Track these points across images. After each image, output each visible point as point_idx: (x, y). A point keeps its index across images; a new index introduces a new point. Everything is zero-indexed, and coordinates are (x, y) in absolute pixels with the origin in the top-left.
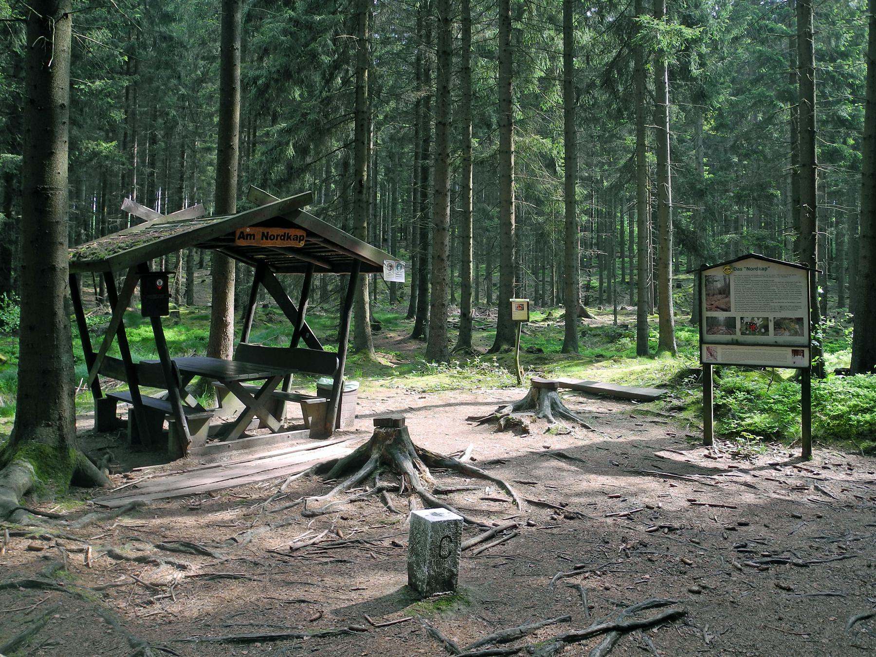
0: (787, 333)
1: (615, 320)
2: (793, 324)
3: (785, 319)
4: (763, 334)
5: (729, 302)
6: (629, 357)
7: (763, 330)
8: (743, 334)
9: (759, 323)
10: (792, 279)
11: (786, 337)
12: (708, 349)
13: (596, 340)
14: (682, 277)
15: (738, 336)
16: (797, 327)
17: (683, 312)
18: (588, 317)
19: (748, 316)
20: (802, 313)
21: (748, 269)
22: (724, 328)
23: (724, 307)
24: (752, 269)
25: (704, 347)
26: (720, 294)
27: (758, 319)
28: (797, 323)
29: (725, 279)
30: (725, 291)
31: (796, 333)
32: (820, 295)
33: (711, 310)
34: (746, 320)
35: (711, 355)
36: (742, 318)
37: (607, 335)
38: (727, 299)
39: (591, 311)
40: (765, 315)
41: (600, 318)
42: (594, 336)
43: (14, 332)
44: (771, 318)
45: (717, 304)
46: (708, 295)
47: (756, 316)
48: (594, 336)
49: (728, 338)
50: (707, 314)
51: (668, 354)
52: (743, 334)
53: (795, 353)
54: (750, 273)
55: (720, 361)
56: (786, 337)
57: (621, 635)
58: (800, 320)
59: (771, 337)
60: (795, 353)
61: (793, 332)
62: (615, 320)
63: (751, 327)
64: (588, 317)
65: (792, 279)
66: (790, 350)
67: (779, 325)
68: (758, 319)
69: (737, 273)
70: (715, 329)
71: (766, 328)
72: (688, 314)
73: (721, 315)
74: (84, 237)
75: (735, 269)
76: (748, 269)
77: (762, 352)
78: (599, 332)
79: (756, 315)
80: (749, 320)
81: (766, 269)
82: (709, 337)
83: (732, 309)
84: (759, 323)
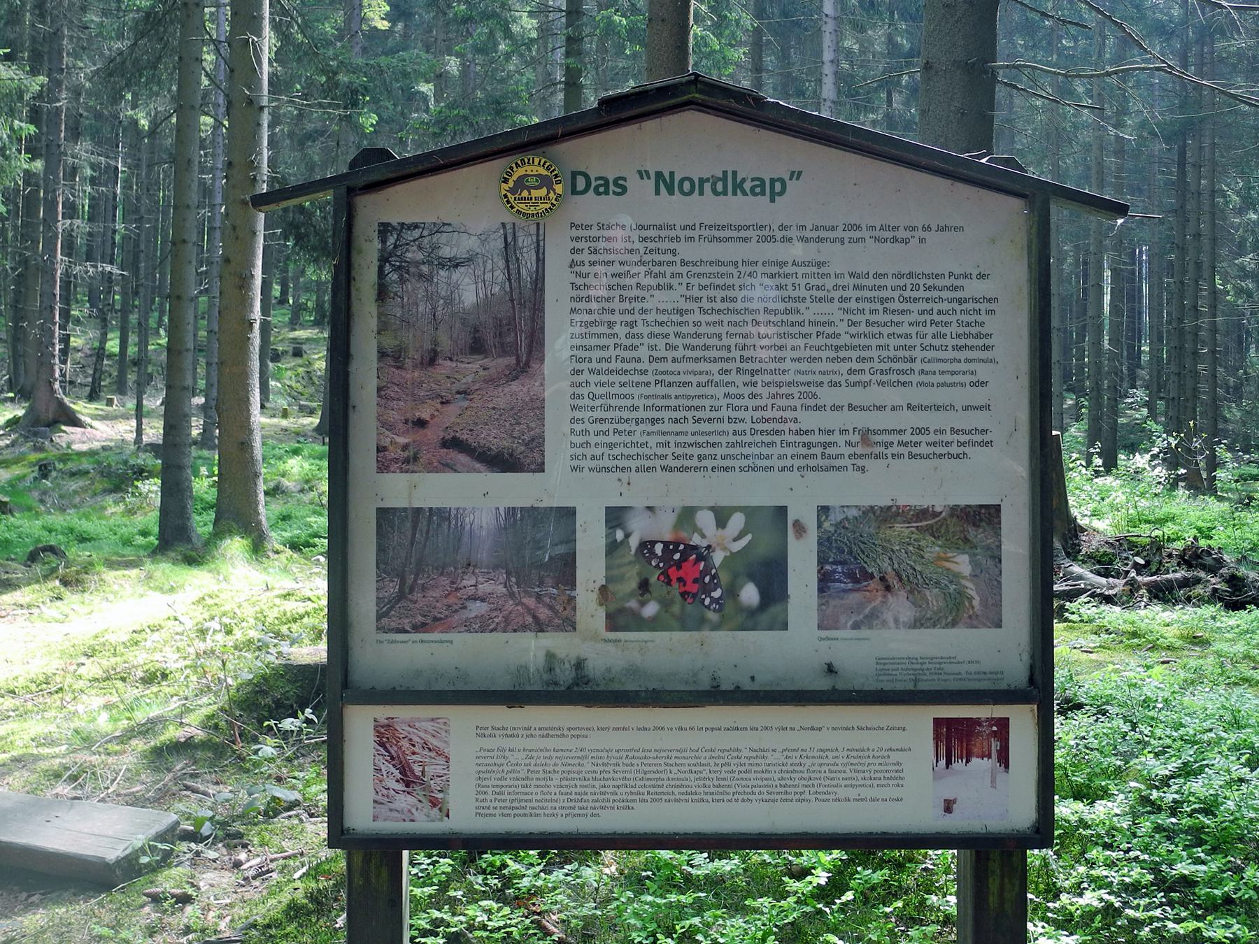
0: (900, 606)
1: (139, 431)
2: (933, 550)
3: (888, 515)
5: (537, 406)
6: (111, 565)
7: (750, 594)
9: (724, 543)
10: (938, 256)
11: (894, 640)
12: (385, 736)
13: (73, 485)
14: (301, 334)
15: (591, 643)
16: (962, 564)
17: (302, 408)
18: (75, 422)
19: (658, 500)
23: (493, 438)
24: (694, 187)
25: (361, 723)
26: (477, 347)
28: (965, 543)
29: (509, 249)
30: (511, 334)
31: (955, 611)
32: (1204, 344)
33: (410, 462)
34: (639, 528)
35: (409, 779)
36: (615, 517)
37: (106, 472)
39: (82, 408)
40: (761, 491)
41: (102, 428)
42: (73, 474)
44: (802, 511)
45: (451, 418)
46: (391, 357)
47: (710, 498)
48: (73, 474)
49: (530, 650)
51: (235, 546)
53: (955, 740)
54: (675, 209)
55: (464, 816)
56: (894, 640)
58: (987, 516)
59: (802, 637)
60: (955, 740)
61: (933, 596)
62: (139, 431)
63: (676, 573)
64: (75, 422)
65: (938, 256)
66: (918, 723)
67: (853, 562)
69: (588, 207)
70: (434, 596)
72: (311, 412)
75: (579, 183)
76: (665, 183)
77: (744, 742)
78: (86, 464)
80: (663, 528)
81: (771, 189)
83: (557, 451)
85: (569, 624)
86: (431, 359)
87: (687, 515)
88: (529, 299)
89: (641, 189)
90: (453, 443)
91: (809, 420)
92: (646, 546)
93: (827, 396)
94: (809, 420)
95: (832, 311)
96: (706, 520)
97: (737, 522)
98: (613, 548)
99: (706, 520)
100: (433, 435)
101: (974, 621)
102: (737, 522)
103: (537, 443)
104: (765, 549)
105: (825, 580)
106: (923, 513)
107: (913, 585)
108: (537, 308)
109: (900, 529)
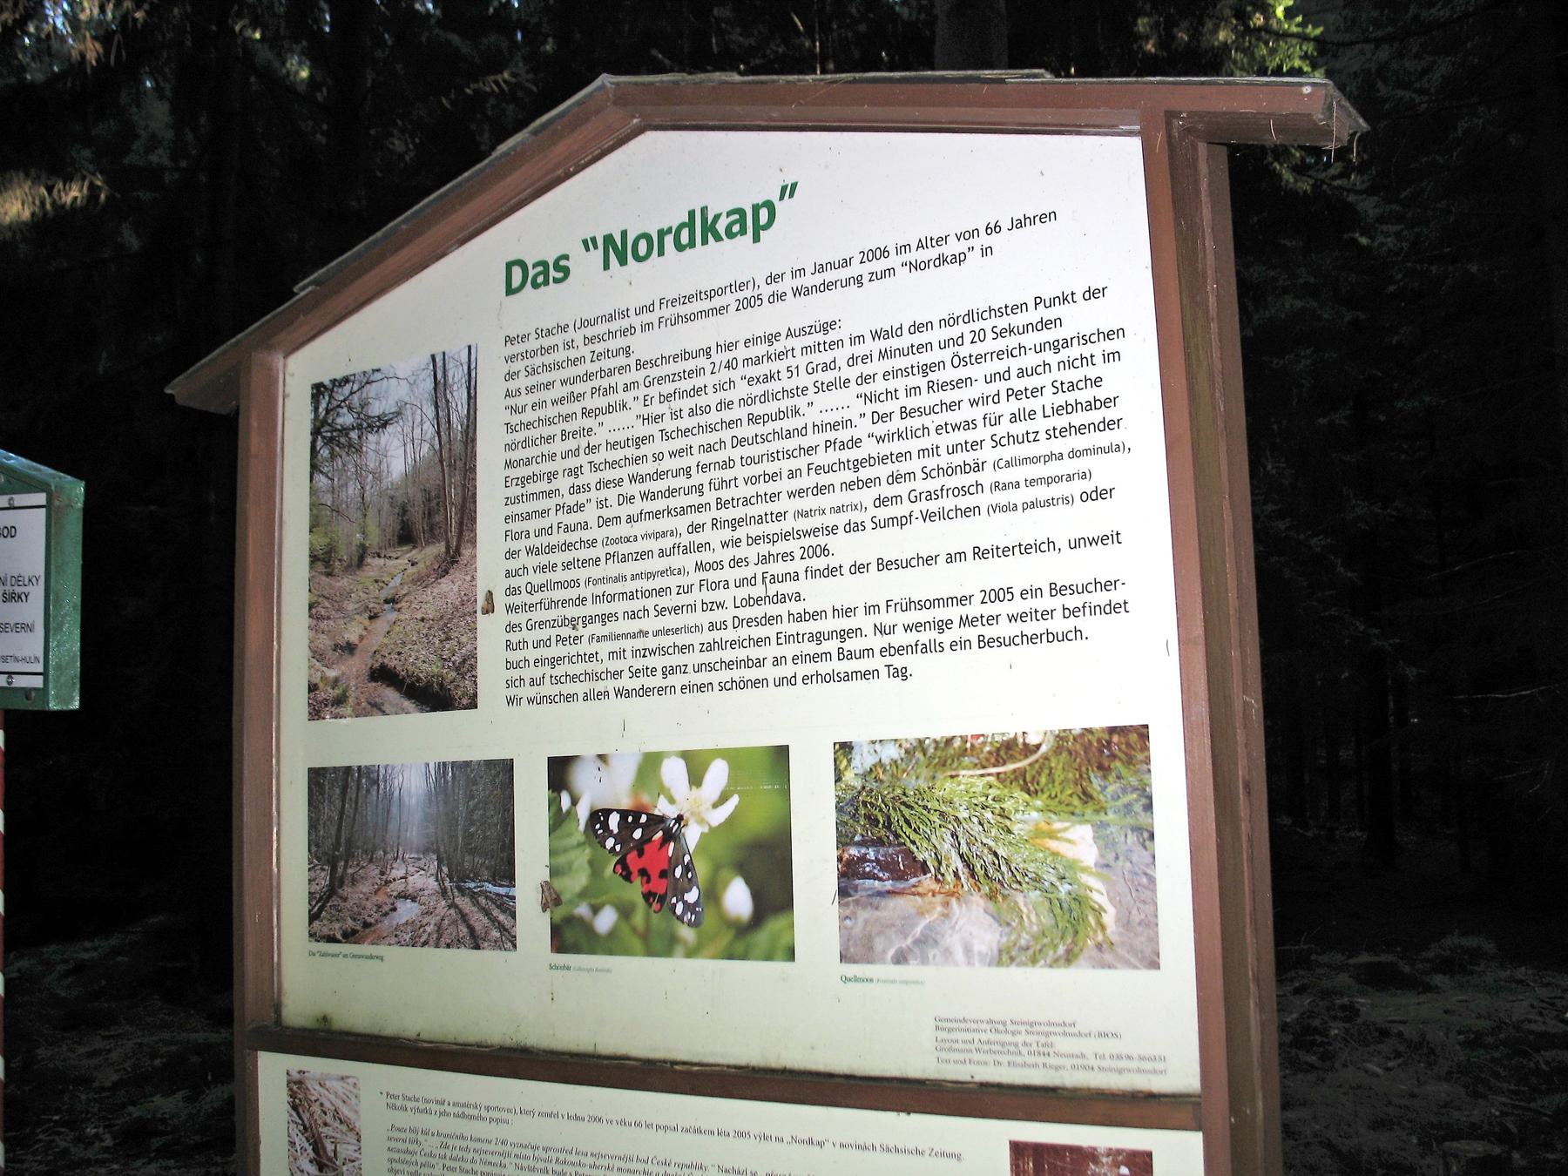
2: (1027, 816)
3: (944, 755)
4: (742, 940)
5: (1110, 1152)
7: (738, 898)
9: (702, 811)
16: (1079, 842)
21: (617, 249)
23: (423, 663)
26: (406, 537)
27: (696, 767)
31: (1069, 932)
36: (559, 771)
40: (746, 721)
52: (569, 936)
57: (1376, 48)
58: (1120, 749)
68: (696, 767)
71: (767, 863)
73: (407, 748)
74: (614, 821)
83: (490, 677)
87: (650, 764)
88: (457, 455)
89: (586, 264)
90: (383, 674)
91: (818, 594)
92: (599, 817)
93: (845, 549)
94: (818, 594)
95: (846, 402)
96: (674, 772)
97: (717, 774)
98: (559, 820)
99: (674, 772)
101: (1107, 954)
102: (717, 774)
103: (467, 666)
104: (758, 822)
105: (849, 872)
106: (1008, 749)
108: (469, 470)
109: (970, 781)
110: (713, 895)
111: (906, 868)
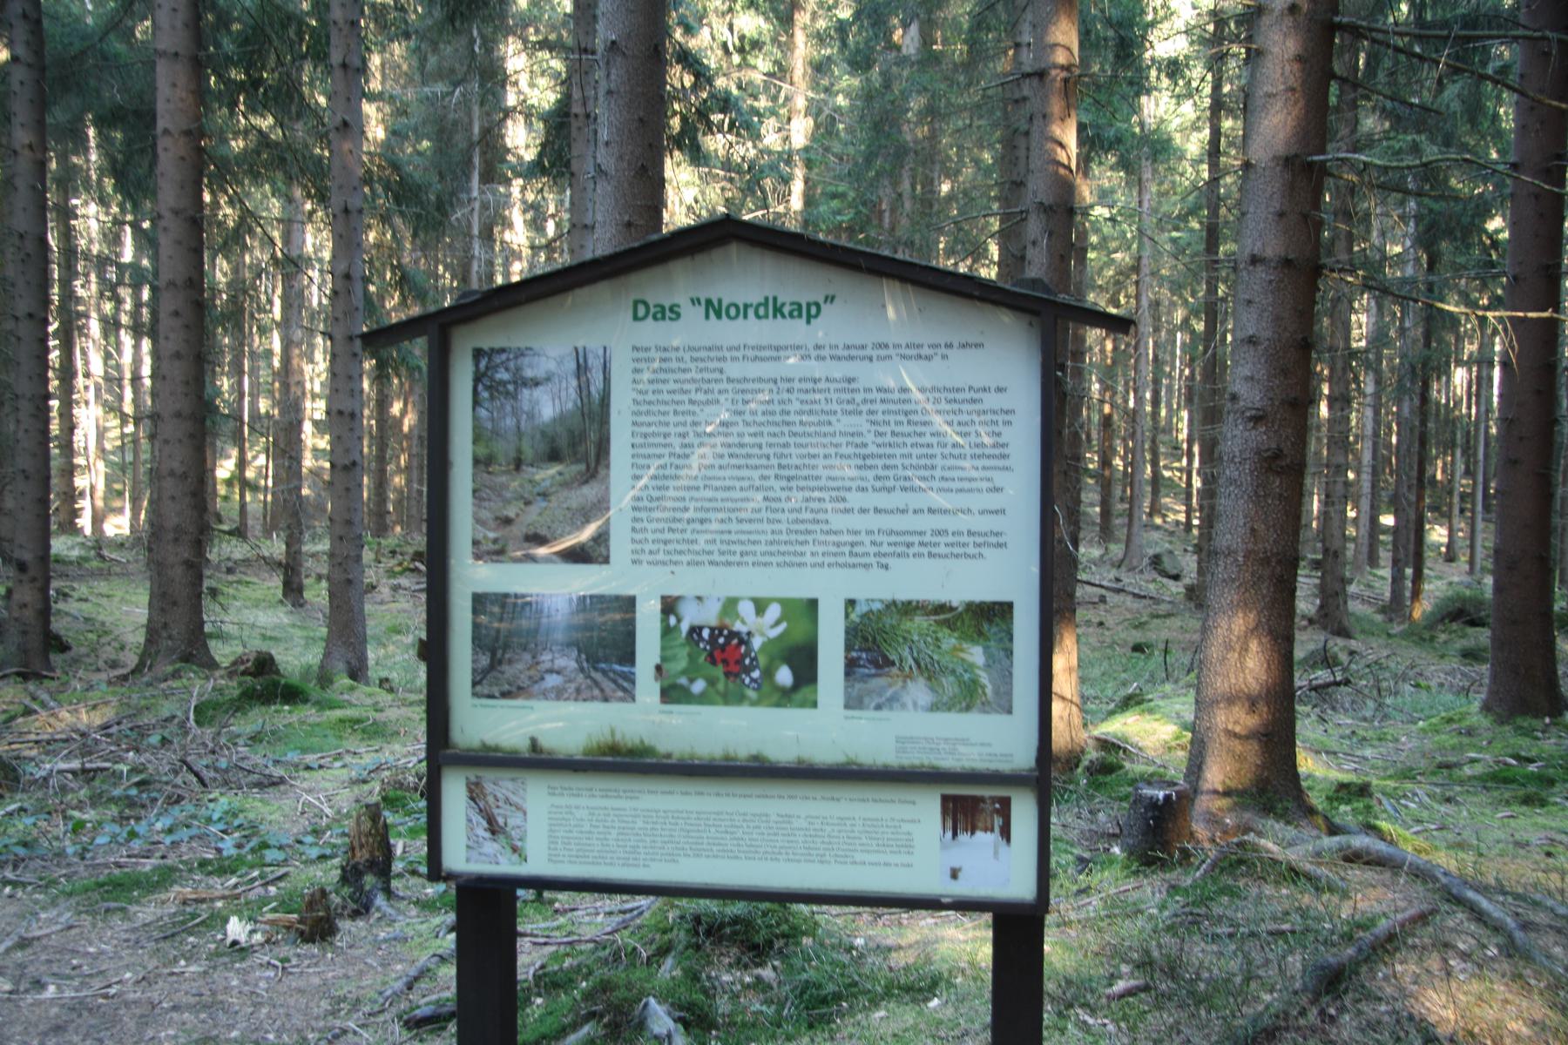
2: (949, 641)
3: (908, 609)
4: (785, 697)
7: (784, 676)
8: (672, 694)
9: (763, 629)
12: (475, 793)
14: (854, 654)
15: (643, 717)
16: (976, 654)
19: (707, 591)
20: (1011, 576)
22: (568, 662)
26: (554, 456)
28: (979, 636)
30: (582, 444)
31: (968, 697)
33: (497, 553)
34: (691, 615)
35: (494, 829)
36: (669, 606)
38: (589, 492)
40: (798, 585)
43: (524, 935)
47: (740, 586)
50: (472, 576)
52: (672, 694)
61: (949, 684)
63: (719, 660)
67: (875, 645)
68: (760, 606)
70: (517, 669)
71: (804, 659)
79: (747, 582)
80: (708, 615)
82: (482, 721)
83: (619, 546)
84: (763, 629)
85: (630, 696)
86: (518, 464)
87: (731, 604)
91: (838, 522)
92: (695, 630)
94: (838, 522)
95: (861, 423)
96: (746, 609)
97: (774, 611)
98: (667, 631)
99: (746, 609)
100: (518, 530)
101: (986, 707)
102: (774, 611)
104: (799, 636)
105: (851, 666)
106: (941, 608)
107: (929, 671)
109: (920, 622)
110: (769, 673)
111: (882, 663)
